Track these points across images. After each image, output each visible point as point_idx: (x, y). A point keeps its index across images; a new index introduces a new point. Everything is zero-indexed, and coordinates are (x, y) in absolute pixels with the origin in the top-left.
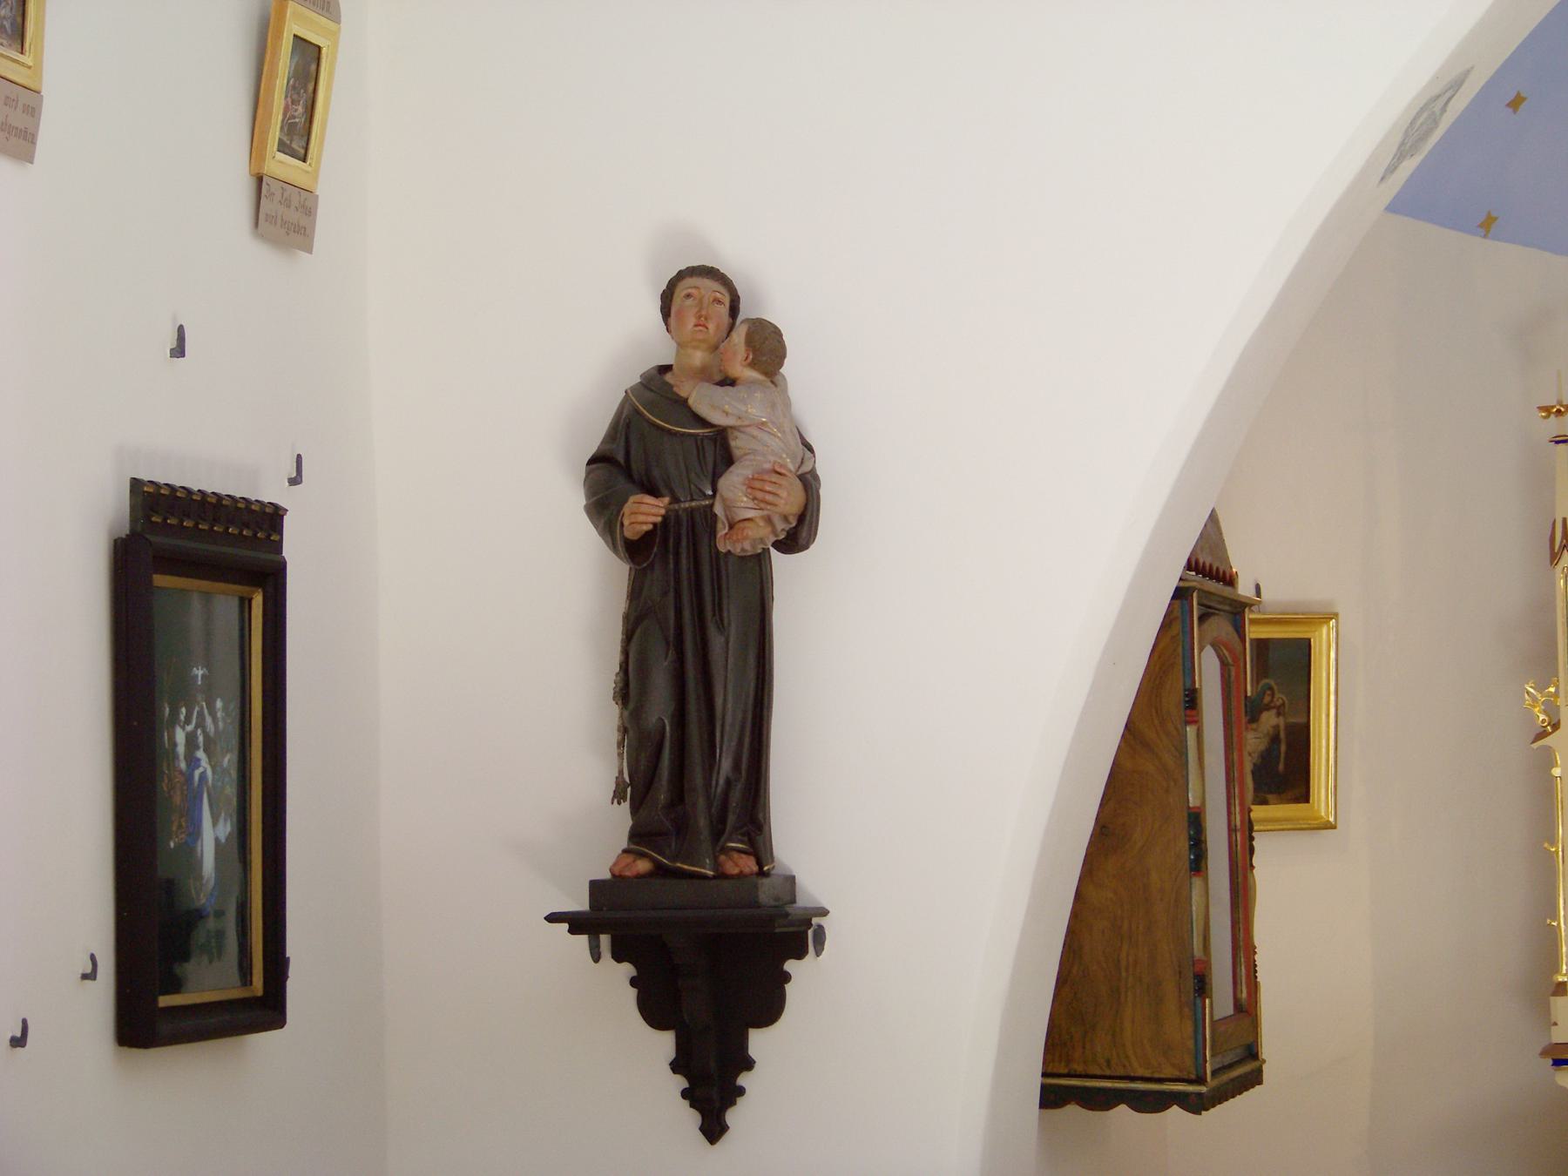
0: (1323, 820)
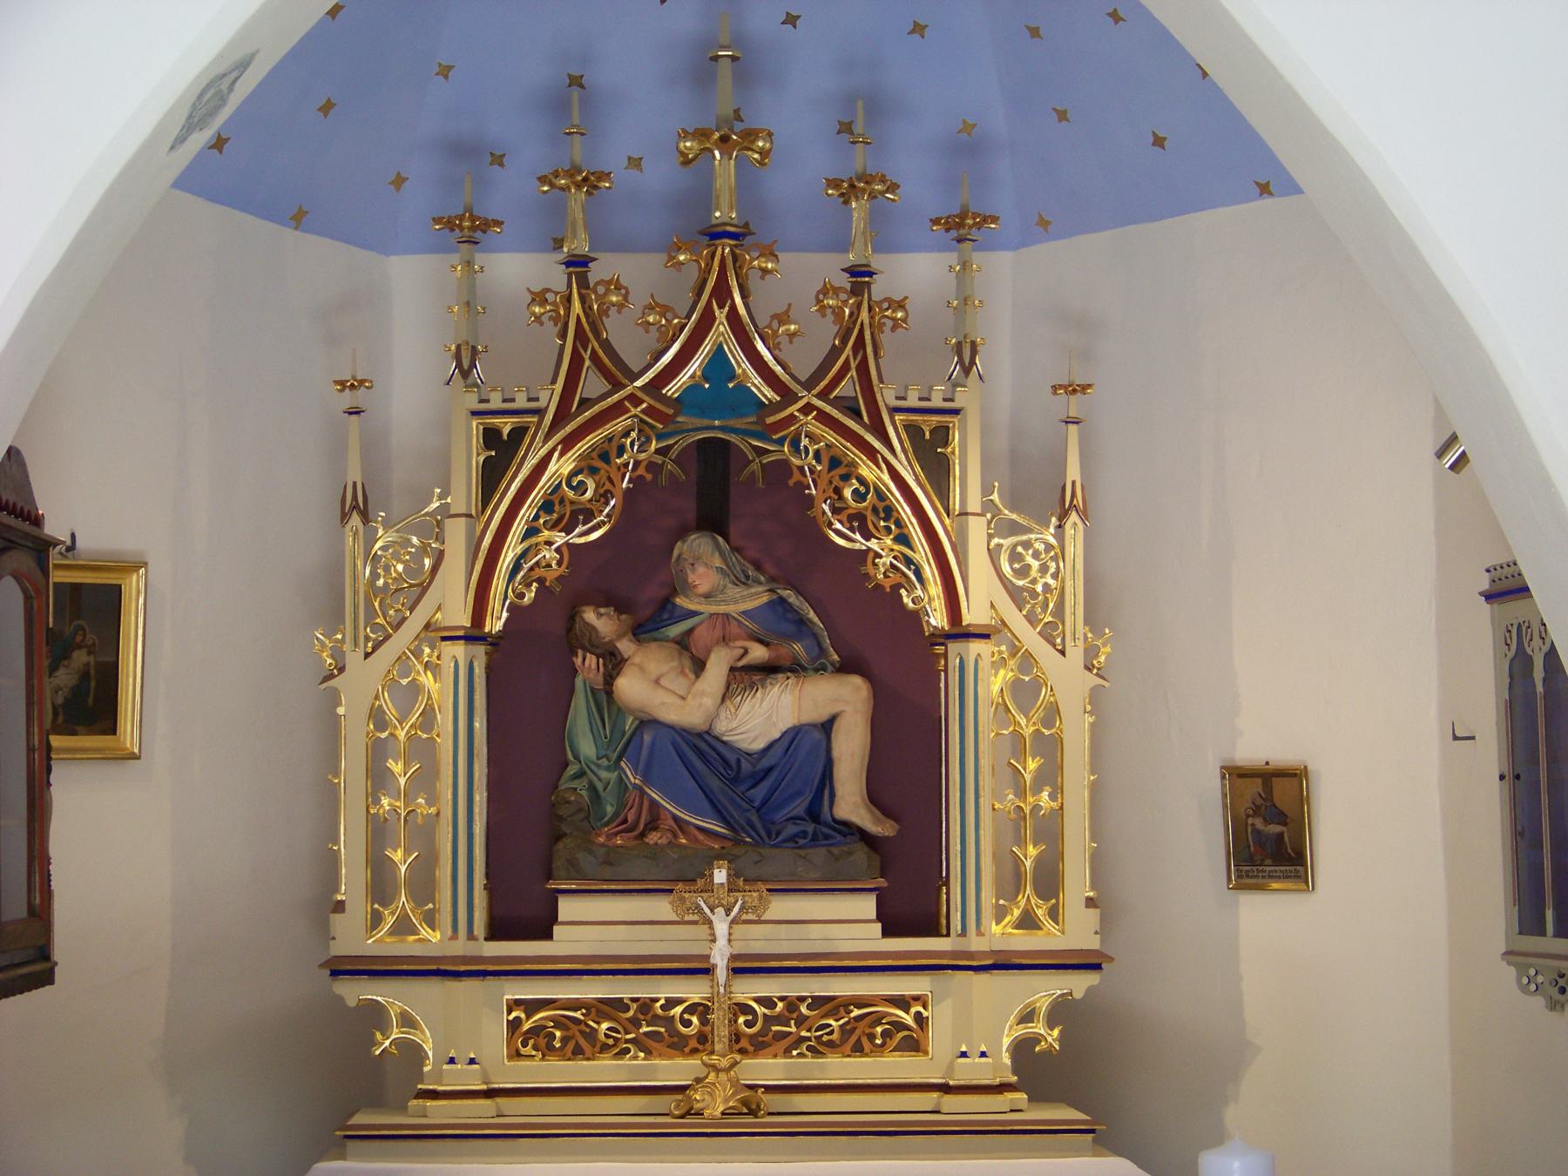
0: (127, 751)
